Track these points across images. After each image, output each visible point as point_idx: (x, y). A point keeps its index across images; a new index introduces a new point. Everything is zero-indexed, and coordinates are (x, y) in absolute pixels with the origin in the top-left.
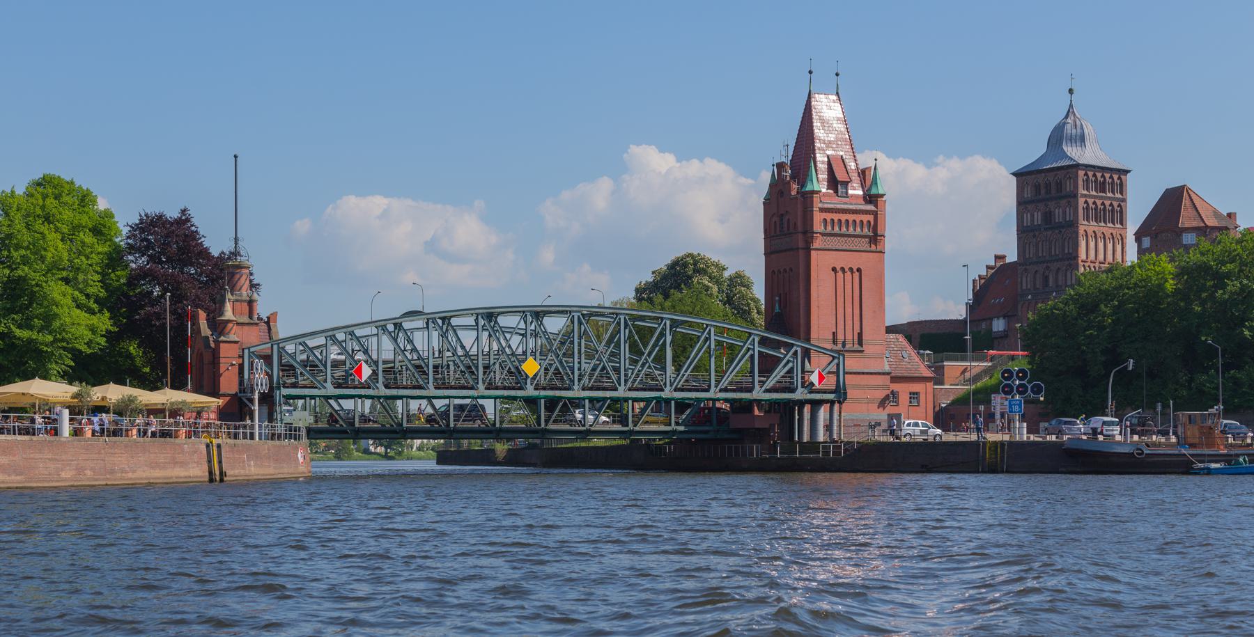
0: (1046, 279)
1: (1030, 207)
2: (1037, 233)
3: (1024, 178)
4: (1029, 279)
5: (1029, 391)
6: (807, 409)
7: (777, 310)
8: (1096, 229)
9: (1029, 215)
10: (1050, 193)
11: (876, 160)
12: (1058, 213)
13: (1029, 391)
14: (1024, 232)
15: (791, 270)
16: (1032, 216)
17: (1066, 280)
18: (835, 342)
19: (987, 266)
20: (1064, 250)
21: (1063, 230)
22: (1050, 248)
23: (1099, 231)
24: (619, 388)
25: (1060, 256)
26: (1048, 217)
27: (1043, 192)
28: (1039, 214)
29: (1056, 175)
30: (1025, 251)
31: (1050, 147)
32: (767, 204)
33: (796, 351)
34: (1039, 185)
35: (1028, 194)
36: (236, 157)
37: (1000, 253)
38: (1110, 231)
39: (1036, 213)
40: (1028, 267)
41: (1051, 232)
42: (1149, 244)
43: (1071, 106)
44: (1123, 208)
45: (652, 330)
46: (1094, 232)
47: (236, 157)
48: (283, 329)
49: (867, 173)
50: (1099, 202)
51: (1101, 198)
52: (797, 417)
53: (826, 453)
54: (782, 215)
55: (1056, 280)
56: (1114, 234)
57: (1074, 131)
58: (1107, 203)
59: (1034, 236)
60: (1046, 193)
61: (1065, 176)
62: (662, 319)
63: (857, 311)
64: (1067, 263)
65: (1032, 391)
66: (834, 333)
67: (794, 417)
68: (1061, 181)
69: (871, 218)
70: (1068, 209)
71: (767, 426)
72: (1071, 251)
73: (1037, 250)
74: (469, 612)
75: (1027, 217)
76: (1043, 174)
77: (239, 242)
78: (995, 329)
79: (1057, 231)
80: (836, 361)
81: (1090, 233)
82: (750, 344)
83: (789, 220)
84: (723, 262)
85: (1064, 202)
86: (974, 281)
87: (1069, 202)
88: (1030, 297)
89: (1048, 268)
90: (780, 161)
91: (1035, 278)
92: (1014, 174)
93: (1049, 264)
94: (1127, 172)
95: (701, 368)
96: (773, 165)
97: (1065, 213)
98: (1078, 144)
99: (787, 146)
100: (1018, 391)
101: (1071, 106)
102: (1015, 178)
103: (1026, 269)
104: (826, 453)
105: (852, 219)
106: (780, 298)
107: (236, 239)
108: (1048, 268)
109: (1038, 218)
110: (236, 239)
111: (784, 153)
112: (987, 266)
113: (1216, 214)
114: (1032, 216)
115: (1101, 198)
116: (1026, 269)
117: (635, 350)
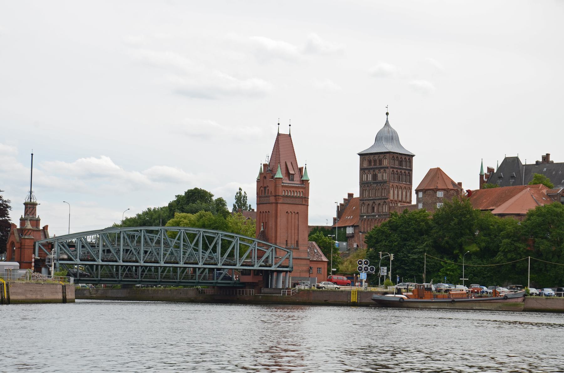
0: (373, 208)
1: (366, 171)
2: (369, 185)
3: (363, 156)
4: (365, 208)
5: (369, 270)
6: (275, 274)
7: (262, 229)
8: (398, 184)
9: (365, 175)
10: (376, 165)
11: (306, 165)
12: (379, 175)
13: (369, 270)
14: (363, 184)
15: (269, 212)
16: (367, 176)
17: (383, 209)
18: (287, 244)
19: (344, 199)
20: (382, 195)
21: (382, 185)
22: (376, 193)
23: (399, 185)
24: (199, 263)
25: (380, 197)
26: (375, 177)
27: (373, 164)
28: (371, 175)
29: (379, 156)
30: (363, 193)
31: (376, 142)
32: (258, 181)
33: (273, 249)
34: (371, 160)
35: (365, 165)
36: (32, 154)
37: (350, 192)
38: (405, 186)
39: (369, 175)
40: (364, 202)
41: (376, 185)
42: (422, 195)
43: (387, 121)
44: (411, 174)
45: (214, 238)
46: (397, 186)
47: (32, 154)
48: (51, 233)
49: (301, 170)
50: (399, 171)
51: (400, 169)
52: (270, 278)
53: (284, 294)
54: (265, 187)
55: (378, 209)
56: (406, 187)
57: (388, 134)
58: (403, 171)
59: (368, 186)
60: (374, 165)
61: (383, 157)
62: (218, 233)
63: (296, 231)
64: (383, 201)
65: (370, 270)
66: (286, 241)
67: (269, 278)
68: (381, 160)
69: (303, 190)
70: (384, 174)
71: (257, 282)
72: (385, 195)
73: (369, 193)
74: (450, 268)
75: (365, 177)
76: (373, 156)
77: (32, 193)
78: (347, 233)
79: (379, 185)
80: (289, 254)
81: (395, 186)
82: (254, 245)
83: (268, 190)
84: (212, 193)
85: (382, 170)
86: (338, 207)
87: (385, 170)
88: (365, 217)
89: (374, 202)
90: (265, 163)
91: (368, 208)
92: (359, 154)
93: (375, 201)
94: (414, 156)
95: (231, 255)
96: (261, 164)
97: (383, 176)
98: (390, 141)
99: (268, 157)
100: (364, 269)
101: (387, 121)
102: (359, 156)
103: (363, 203)
104: (284, 294)
105: (293, 190)
106: (263, 224)
107: (31, 192)
108: (374, 202)
109: (370, 177)
110: (31, 192)
111: (267, 160)
112: (344, 199)
113: (453, 183)
114: (367, 176)
115: (400, 169)
116: (363, 203)
117: (205, 248)
